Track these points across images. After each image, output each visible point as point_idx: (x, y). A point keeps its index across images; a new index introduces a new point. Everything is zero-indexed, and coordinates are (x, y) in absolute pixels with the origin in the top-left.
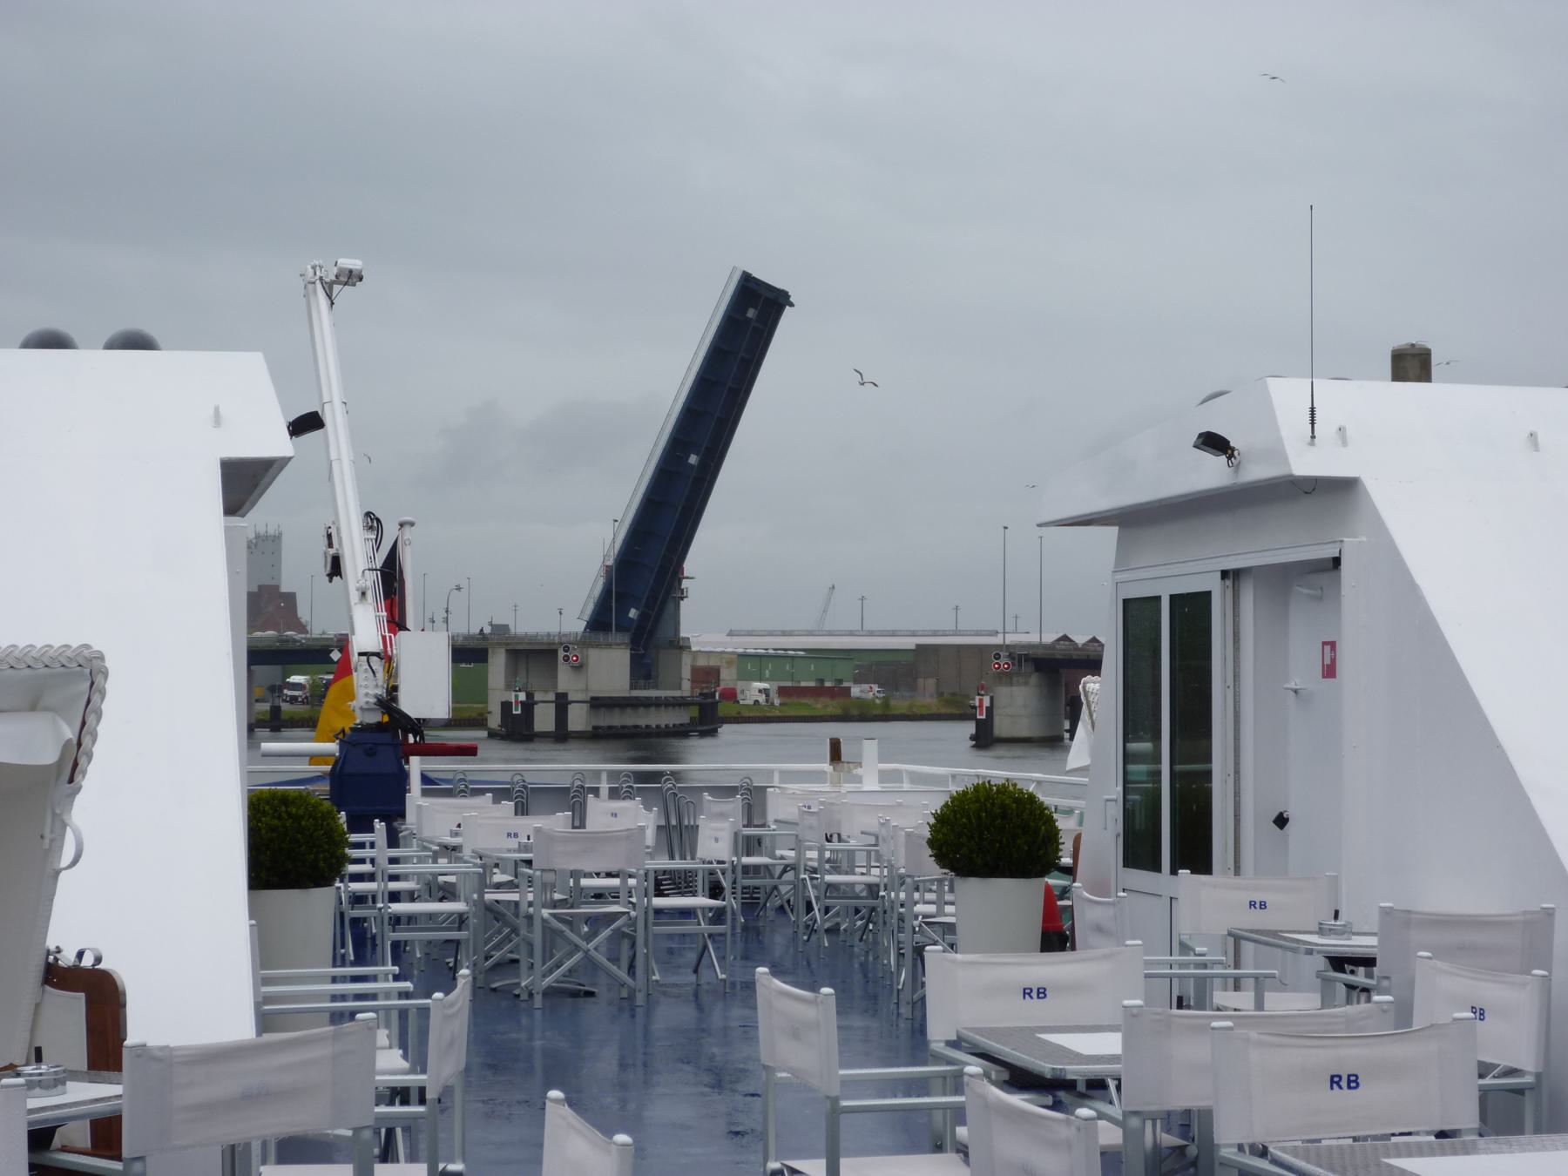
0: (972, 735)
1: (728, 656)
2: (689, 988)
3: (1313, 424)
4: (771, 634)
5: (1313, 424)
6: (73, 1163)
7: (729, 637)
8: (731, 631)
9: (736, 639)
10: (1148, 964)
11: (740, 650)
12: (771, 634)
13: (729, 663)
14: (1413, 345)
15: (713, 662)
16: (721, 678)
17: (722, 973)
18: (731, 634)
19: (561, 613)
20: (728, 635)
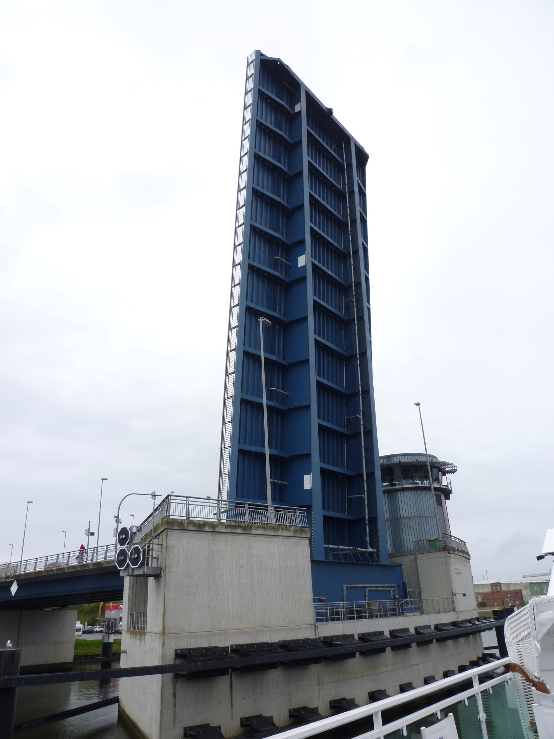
0: (83, 546)
1: (524, 584)
2: (42, 720)
3: (25, 531)
4: (541, 575)
5: (25, 531)
6: (446, 683)
7: (523, 578)
8: (524, 575)
9: (527, 579)
10: (315, 605)
11: (530, 582)
12: (541, 575)
13: (526, 587)
14: (444, 461)
15: (518, 588)
16: (523, 595)
17: (119, 567)
18: (524, 577)
19: (483, 577)
20: (523, 577)
